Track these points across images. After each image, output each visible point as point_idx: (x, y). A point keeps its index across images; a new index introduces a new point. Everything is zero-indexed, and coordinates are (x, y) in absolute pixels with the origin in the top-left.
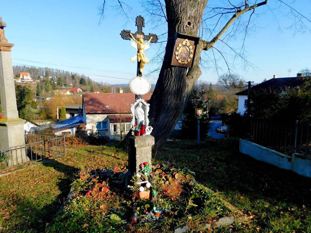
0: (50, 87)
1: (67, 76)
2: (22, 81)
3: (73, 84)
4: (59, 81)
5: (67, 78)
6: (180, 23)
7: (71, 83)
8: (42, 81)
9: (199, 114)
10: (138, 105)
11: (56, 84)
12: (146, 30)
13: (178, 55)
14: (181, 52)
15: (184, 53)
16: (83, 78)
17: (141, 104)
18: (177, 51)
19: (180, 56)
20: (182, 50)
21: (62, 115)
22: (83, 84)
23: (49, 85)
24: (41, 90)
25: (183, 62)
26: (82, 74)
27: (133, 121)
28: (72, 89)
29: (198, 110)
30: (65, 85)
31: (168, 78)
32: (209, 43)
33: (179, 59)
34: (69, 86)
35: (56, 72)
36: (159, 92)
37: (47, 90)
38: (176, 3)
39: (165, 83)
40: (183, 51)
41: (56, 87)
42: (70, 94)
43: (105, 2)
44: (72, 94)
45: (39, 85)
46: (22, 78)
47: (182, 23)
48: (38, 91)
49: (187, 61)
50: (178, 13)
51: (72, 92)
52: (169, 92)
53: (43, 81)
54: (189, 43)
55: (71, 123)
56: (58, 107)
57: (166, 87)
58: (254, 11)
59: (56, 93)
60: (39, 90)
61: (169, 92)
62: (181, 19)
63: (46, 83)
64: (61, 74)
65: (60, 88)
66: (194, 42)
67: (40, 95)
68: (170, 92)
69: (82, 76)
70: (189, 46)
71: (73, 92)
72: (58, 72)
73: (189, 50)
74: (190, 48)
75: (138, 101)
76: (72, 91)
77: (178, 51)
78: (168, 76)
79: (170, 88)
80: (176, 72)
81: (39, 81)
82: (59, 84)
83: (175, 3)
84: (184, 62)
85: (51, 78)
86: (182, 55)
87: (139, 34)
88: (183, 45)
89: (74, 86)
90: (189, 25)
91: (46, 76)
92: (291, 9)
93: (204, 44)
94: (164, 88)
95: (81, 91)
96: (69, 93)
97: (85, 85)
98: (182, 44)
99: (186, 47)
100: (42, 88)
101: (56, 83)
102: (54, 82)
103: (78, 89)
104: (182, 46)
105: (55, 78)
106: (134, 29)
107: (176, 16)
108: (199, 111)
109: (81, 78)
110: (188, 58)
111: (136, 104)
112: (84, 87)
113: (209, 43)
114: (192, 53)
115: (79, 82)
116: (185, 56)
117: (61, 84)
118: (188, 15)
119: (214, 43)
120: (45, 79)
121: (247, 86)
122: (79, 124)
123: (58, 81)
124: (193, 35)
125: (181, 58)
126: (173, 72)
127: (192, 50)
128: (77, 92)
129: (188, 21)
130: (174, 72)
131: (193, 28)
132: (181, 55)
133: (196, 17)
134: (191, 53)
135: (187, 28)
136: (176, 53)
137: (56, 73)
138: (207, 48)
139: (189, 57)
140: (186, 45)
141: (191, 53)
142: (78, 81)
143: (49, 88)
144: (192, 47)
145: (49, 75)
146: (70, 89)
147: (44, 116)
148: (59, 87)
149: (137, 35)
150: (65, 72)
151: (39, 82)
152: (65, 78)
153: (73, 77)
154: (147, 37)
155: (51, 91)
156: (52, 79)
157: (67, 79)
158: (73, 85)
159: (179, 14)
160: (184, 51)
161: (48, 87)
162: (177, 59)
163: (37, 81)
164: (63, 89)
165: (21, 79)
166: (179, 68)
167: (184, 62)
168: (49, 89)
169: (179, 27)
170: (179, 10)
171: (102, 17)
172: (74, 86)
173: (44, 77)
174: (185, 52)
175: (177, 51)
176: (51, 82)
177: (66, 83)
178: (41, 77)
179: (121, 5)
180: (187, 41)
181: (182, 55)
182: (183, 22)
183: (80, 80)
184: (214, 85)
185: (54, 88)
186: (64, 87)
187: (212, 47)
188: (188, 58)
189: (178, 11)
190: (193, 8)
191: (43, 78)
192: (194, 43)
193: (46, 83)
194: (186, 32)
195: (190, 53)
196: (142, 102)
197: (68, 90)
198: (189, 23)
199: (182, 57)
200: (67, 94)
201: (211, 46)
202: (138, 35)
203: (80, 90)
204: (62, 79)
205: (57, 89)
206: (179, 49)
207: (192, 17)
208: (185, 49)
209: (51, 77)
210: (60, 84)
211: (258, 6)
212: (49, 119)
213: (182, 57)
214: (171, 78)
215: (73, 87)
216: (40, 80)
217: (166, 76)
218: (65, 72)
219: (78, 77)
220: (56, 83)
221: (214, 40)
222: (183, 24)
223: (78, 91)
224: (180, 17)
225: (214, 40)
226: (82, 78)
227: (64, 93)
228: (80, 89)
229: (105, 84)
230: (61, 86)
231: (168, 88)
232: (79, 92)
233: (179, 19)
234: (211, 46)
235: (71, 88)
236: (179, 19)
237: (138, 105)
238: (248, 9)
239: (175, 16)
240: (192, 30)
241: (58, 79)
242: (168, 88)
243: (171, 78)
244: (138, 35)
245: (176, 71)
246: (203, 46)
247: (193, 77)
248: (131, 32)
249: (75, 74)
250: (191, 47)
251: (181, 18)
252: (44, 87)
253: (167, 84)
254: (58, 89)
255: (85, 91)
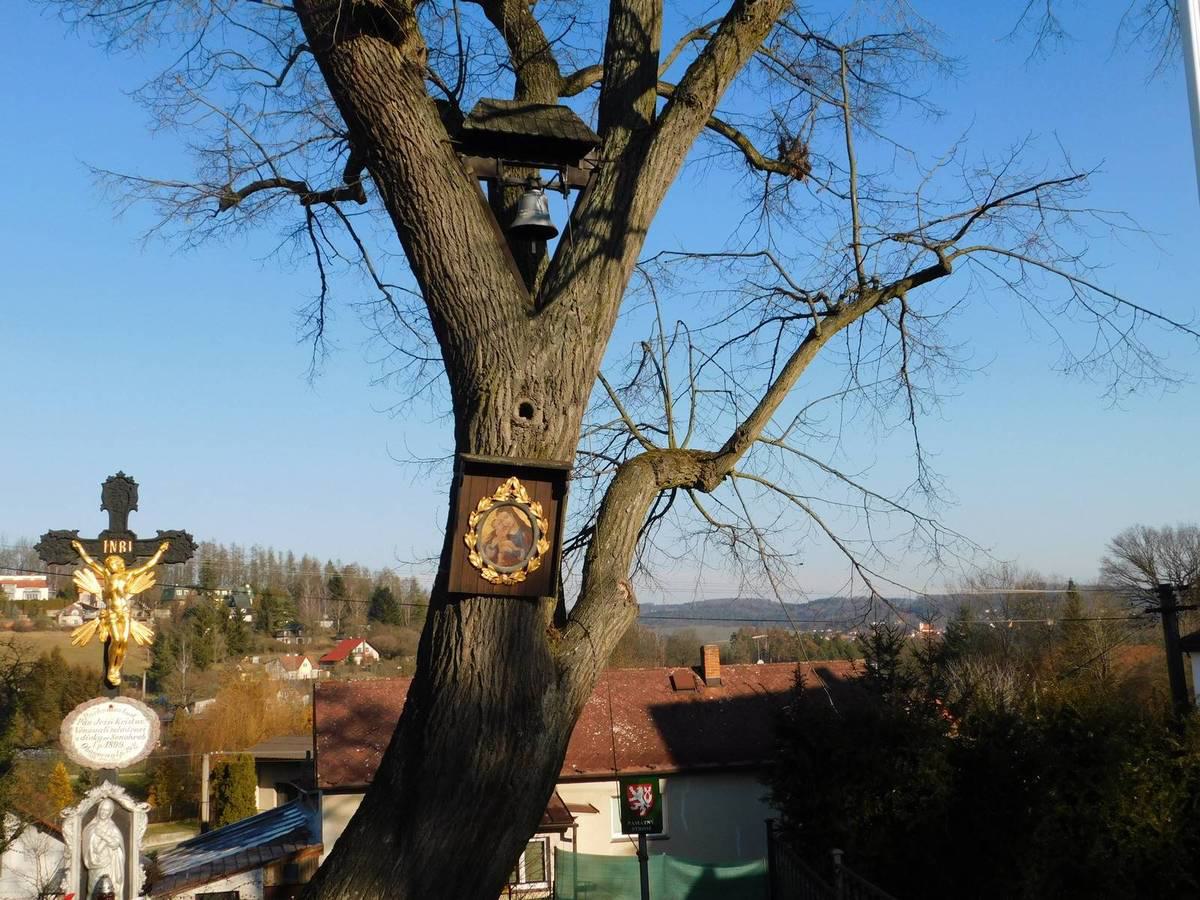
0: (220, 641)
1: (307, 582)
2: (87, 617)
3: (335, 621)
4: (264, 608)
5: (308, 590)
6: (485, 413)
7: (326, 617)
8: (180, 613)
9: (637, 805)
10: (93, 812)
11: (248, 623)
12: (143, 524)
13: (481, 549)
14: (494, 534)
15: (509, 537)
16: (387, 589)
17: (107, 807)
18: (472, 531)
19: (488, 550)
20: (496, 523)
21: (236, 794)
22: (383, 622)
23: (216, 631)
24: (173, 659)
25: (505, 577)
26: (380, 569)
27: (69, 879)
28: (329, 646)
29: (631, 788)
30: (295, 629)
31: (445, 650)
32: (714, 460)
33: (485, 565)
34: (315, 630)
35: (254, 564)
36: (417, 711)
37: (200, 662)
38: (464, 333)
39: (436, 671)
40: (500, 527)
41: (249, 644)
42: (315, 676)
43: (324, 289)
44: (328, 673)
45: (166, 634)
46: (88, 603)
47: (491, 410)
48: (155, 667)
49: (525, 569)
50: (474, 375)
51: (326, 663)
52: (449, 713)
53: (189, 612)
54: (523, 490)
55: (253, 843)
56: (206, 757)
57: (439, 689)
58: (904, 306)
59: (244, 675)
60: (165, 662)
61: (449, 713)
62: (488, 398)
63: (199, 623)
64: (275, 574)
65: (266, 647)
66: (550, 485)
67: (166, 686)
68: (454, 712)
69: (381, 580)
70: (529, 505)
71: (331, 663)
72: (263, 565)
73: (528, 523)
74: (535, 513)
75: (95, 793)
76: (328, 659)
77: (475, 530)
78: (445, 640)
79: (455, 692)
80: (477, 619)
81: (168, 613)
82: (262, 624)
83: (460, 333)
84: (508, 574)
85: (226, 597)
86: (497, 547)
87: (112, 539)
88: (498, 504)
89: (340, 631)
90: (524, 418)
91: (205, 588)
92: (1072, 286)
93: (656, 474)
94: (434, 692)
95: (376, 655)
96: (313, 668)
97: (396, 623)
98: (494, 501)
99: (514, 508)
100: (176, 651)
101: (248, 618)
102: (239, 617)
103: (361, 646)
104: (492, 509)
105: (245, 593)
106: (93, 522)
107: (470, 386)
108: (640, 789)
109: (378, 589)
110: (527, 554)
111: (84, 806)
112: (390, 636)
113: (714, 460)
114: (545, 532)
115: (365, 608)
116: (511, 550)
117: (275, 624)
118: (519, 376)
119: (733, 456)
120: (199, 601)
121: (1184, 608)
122: (290, 848)
123: (259, 607)
124: (543, 463)
125: (494, 559)
126: (464, 621)
127: (543, 521)
128: (355, 663)
129: (521, 401)
130: (471, 622)
131: (546, 428)
132: (493, 545)
133: (559, 383)
134: (537, 533)
135: (515, 428)
136: (467, 541)
137: (255, 571)
138: (705, 483)
139: (533, 551)
140: (510, 504)
141: (537, 533)
142: (360, 609)
143: (215, 647)
144: (539, 508)
145: (216, 581)
146: (320, 648)
147: (160, 800)
148: (263, 639)
149: (106, 542)
150: (298, 559)
151: (166, 620)
152: (297, 592)
153: (337, 585)
154: (148, 544)
155: (219, 661)
156: (230, 602)
157: (306, 601)
158: (335, 625)
159: (478, 378)
160: (505, 527)
161: (208, 642)
162: (475, 564)
163: (157, 612)
164: (284, 649)
165: (83, 605)
166: (491, 603)
167: (511, 576)
168: (212, 652)
169: (480, 426)
170: (478, 362)
171: (321, 349)
172: (341, 633)
173: (194, 592)
174: (513, 533)
175: (472, 531)
176: (224, 615)
177: (299, 620)
178: (179, 592)
179: (389, 297)
180: (515, 486)
181: (497, 547)
182: (497, 409)
183: (372, 596)
184: (1087, 589)
185: (239, 646)
186: (287, 639)
187: (729, 473)
188: (527, 554)
189: (474, 366)
190: (538, 347)
191: (189, 599)
192: (549, 492)
193: (199, 623)
194: (511, 447)
195: (530, 534)
196: (115, 797)
197: (307, 653)
198: (527, 411)
199: (500, 556)
200: (301, 677)
201: (721, 469)
202: (109, 543)
203: (371, 649)
204: (281, 600)
205: (253, 651)
206: (481, 522)
207: (536, 382)
208: (510, 520)
209: (225, 593)
210: (271, 626)
211: (914, 285)
212: (188, 820)
213: (498, 552)
214: (456, 649)
215: (334, 639)
216: (172, 611)
217: (439, 638)
218: (298, 559)
219: (363, 585)
220: (248, 618)
221: (733, 447)
222: (496, 416)
223: (358, 659)
224: (481, 389)
225: (733, 447)
226: (383, 586)
227: (287, 670)
228: (367, 645)
229: (160, 686)
230: (275, 637)
231: (449, 692)
232: (362, 662)
233: (479, 399)
234: (721, 469)
235: (324, 641)
236: (480, 396)
237: (93, 812)
238: (874, 299)
239: (466, 384)
240: (540, 437)
241: (260, 597)
242: (449, 692)
243: (456, 649)
244: (109, 543)
245: (480, 617)
246: (653, 482)
247: (587, 634)
248: (79, 535)
249: (348, 570)
250: (536, 509)
251: (488, 391)
252: (188, 646)
253: (445, 673)
254: (257, 654)
255: (393, 655)
